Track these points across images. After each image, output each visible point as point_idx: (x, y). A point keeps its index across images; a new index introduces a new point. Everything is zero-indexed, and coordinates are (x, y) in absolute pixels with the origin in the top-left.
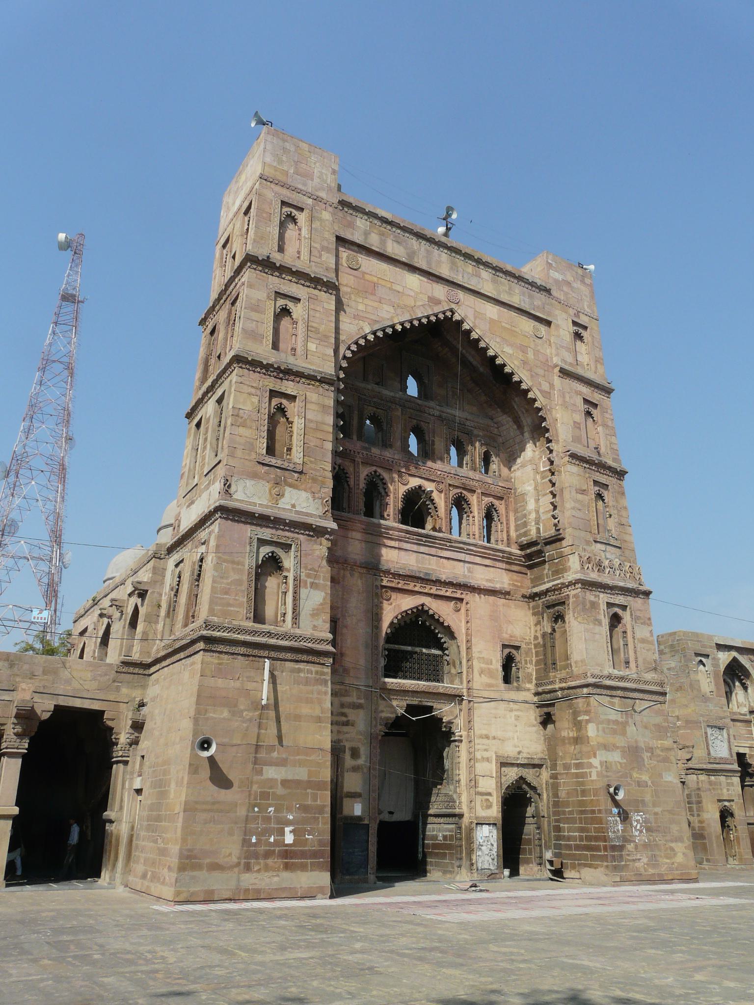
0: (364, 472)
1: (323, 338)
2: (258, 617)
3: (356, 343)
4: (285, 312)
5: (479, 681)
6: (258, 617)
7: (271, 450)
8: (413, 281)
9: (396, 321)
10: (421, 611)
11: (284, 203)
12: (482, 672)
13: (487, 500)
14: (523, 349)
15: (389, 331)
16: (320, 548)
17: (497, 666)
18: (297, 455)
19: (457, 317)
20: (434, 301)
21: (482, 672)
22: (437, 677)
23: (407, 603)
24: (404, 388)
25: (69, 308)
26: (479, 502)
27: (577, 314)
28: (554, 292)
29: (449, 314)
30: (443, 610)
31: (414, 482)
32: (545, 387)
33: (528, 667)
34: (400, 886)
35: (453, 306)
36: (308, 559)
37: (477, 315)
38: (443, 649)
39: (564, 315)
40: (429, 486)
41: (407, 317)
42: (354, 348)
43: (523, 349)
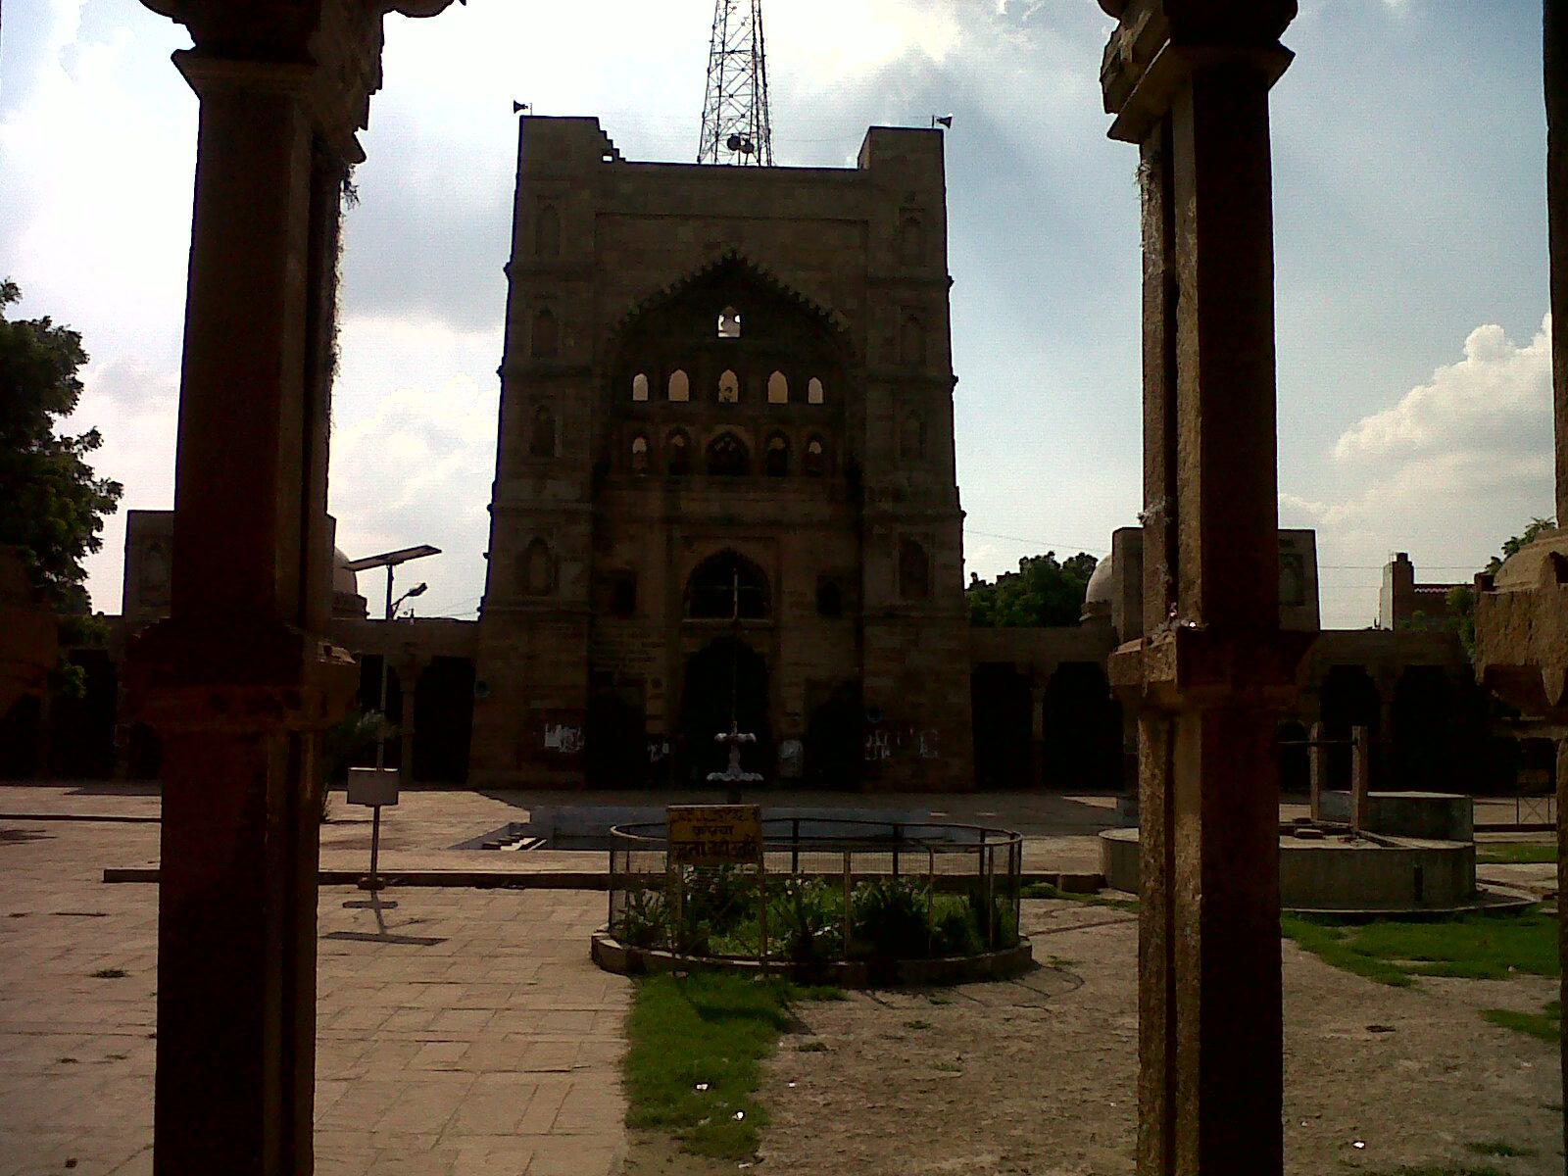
31: (720, 429)
40: (740, 431)
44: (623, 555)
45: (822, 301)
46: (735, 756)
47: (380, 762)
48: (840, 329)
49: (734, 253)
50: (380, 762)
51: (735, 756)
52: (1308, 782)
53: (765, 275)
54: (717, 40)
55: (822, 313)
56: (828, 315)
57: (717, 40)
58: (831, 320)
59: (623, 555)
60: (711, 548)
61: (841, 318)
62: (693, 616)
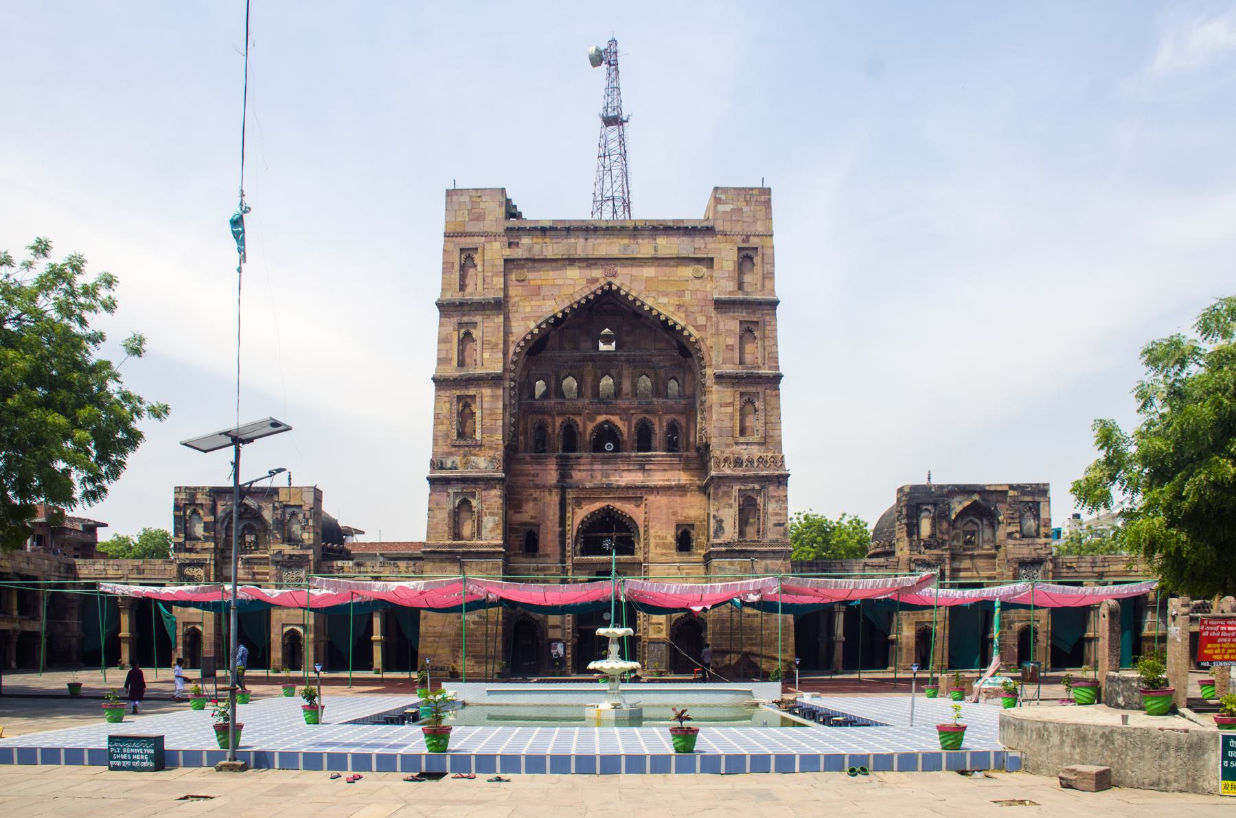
0: (559, 421)
1: (494, 347)
2: (457, 535)
3: (524, 339)
5: (653, 553)
6: (457, 535)
7: (461, 435)
8: (573, 273)
9: (557, 310)
10: (608, 511)
11: (462, 250)
12: (657, 546)
13: (668, 418)
15: (552, 321)
16: (496, 493)
17: (670, 536)
18: (478, 436)
19: (614, 288)
21: (657, 546)
26: (660, 421)
28: (718, 228)
29: (606, 288)
30: (627, 508)
31: (601, 418)
32: (701, 320)
33: (698, 538)
35: (609, 279)
36: (490, 503)
37: (633, 279)
38: (628, 531)
39: (729, 246)
40: (616, 419)
41: (567, 303)
42: (522, 344)
43: (680, 294)
44: (528, 513)
45: (679, 319)
46: (614, 649)
47: (498, 769)
48: (692, 339)
49: (610, 284)
50: (498, 769)
51: (614, 649)
52: (917, 764)
53: (635, 299)
54: (598, 192)
55: (678, 328)
56: (683, 329)
57: (598, 192)
58: (685, 333)
59: (528, 513)
60: (598, 505)
61: (691, 330)
62: (582, 555)
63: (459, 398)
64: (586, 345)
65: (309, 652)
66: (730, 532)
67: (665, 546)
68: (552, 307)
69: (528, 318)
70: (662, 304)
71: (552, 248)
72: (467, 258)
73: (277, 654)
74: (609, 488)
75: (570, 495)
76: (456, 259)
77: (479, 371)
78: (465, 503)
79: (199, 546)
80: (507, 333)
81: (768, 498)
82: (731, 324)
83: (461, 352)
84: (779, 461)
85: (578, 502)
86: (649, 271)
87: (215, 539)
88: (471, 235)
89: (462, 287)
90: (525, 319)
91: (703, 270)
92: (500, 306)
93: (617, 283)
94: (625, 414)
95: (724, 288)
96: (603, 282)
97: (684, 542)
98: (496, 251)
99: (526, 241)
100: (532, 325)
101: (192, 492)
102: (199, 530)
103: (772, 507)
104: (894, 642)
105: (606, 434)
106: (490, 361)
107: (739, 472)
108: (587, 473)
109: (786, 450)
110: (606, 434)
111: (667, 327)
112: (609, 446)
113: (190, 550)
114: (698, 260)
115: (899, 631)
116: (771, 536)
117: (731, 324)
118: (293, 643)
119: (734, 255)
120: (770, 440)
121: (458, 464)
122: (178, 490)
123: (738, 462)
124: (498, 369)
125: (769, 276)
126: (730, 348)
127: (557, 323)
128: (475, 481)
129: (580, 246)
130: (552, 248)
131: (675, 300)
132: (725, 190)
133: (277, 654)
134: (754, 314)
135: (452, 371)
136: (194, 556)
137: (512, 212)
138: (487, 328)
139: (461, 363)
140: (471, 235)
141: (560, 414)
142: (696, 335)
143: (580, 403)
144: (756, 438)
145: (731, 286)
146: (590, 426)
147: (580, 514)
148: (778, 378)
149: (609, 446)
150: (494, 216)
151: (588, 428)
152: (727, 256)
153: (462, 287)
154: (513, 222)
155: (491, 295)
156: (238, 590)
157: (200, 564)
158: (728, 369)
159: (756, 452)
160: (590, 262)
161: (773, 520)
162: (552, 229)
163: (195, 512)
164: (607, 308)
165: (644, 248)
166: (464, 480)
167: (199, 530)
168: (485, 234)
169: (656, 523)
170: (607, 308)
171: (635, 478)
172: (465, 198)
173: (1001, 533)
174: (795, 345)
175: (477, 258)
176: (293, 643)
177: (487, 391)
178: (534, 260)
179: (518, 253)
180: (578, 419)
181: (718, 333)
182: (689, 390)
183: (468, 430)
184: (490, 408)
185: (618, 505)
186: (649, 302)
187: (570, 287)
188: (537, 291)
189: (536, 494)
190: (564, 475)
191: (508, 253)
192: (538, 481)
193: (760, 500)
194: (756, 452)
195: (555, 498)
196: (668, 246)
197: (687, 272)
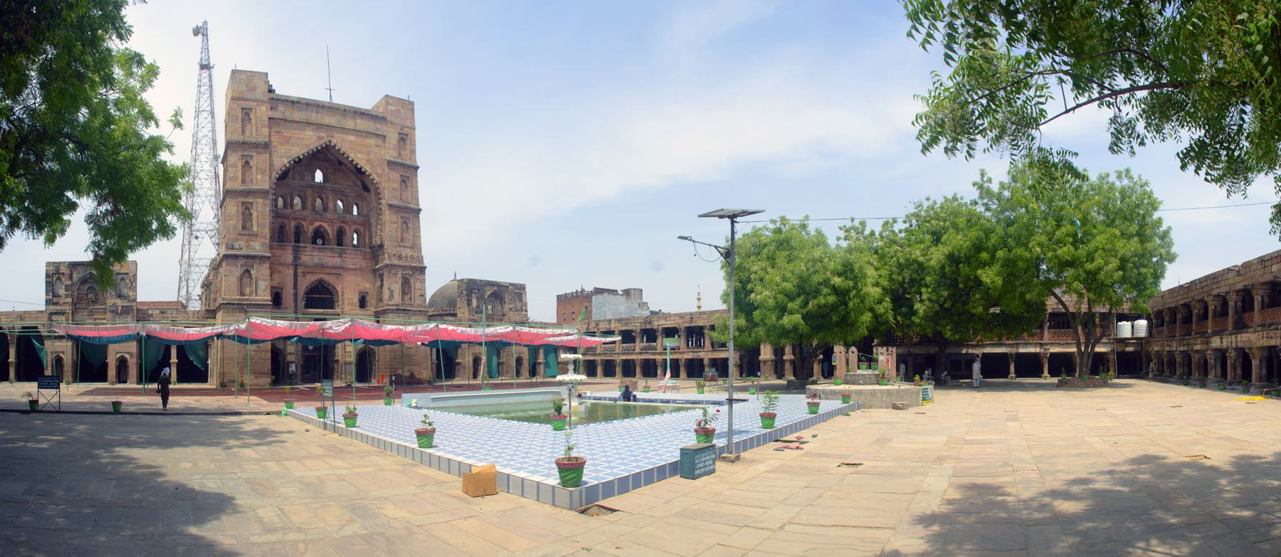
0: (293, 224)
1: (263, 173)
2: (242, 294)
4: (247, 163)
5: (347, 309)
6: (242, 294)
7: (244, 228)
10: (321, 282)
14: (368, 153)
17: (356, 301)
18: (255, 228)
20: (320, 138)
22: (332, 308)
23: (314, 278)
24: (314, 178)
25: (205, 74)
27: (403, 128)
30: (330, 279)
31: (317, 224)
32: (380, 171)
33: (371, 301)
34: (1219, 456)
40: (325, 225)
43: (368, 153)
45: (367, 168)
63: (243, 203)
64: (308, 178)
65: (133, 371)
66: (397, 299)
67: (352, 304)
68: (298, 151)
69: (283, 156)
70: (359, 158)
71: (297, 115)
72: (246, 113)
73: (112, 372)
74: (322, 266)
75: (300, 270)
76: (239, 114)
77: (255, 187)
78: (247, 271)
79: (61, 301)
80: (271, 165)
81: (416, 279)
82: (396, 176)
83: (243, 174)
84: (420, 259)
85: (304, 274)
86: (351, 138)
87: (72, 296)
88: (248, 100)
89: (243, 132)
90: (281, 157)
91: (380, 142)
92: (266, 146)
93: (334, 141)
94: (331, 221)
95: (391, 155)
96: (326, 140)
97: (363, 303)
98: (263, 112)
99: (281, 108)
100: (286, 161)
101: (57, 265)
102: (62, 292)
103: (418, 285)
104: (459, 364)
105: (319, 235)
106: (262, 181)
107: (401, 263)
108: (311, 256)
109: (424, 253)
110: (319, 235)
111: (359, 172)
112: (319, 241)
113: (56, 304)
114: (378, 135)
115: (463, 358)
116: (418, 302)
117: (396, 176)
118: (122, 364)
119: (397, 136)
120: (416, 246)
121: (242, 247)
122: (48, 264)
123: (400, 257)
124: (266, 186)
125: (413, 152)
126: (395, 189)
127: (298, 162)
128: (254, 257)
129: (314, 117)
130: (297, 115)
131: (365, 157)
132: (392, 98)
133: (112, 372)
134: (408, 172)
135: (237, 185)
136: (58, 308)
137: (271, 91)
138: (259, 160)
139: (243, 181)
140: (248, 100)
141: (294, 219)
142: (377, 179)
143: (306, 213)
144: (408, 244)
145: (395, 154)
146: (311, 229)
147: (305, 282)
148: (420, 210)
149: (319, 241)
150: (261, 93)
151: (310, 229)
152: (393, 137)
153: (243, 132)
154: (272, 95)
155: (262, 140)
156: (88, 330)
157: (62, 313)
158: (394, 202)
159: (409, 252)
160: (319, 126)
161: (418, 293)
162: (298, 102)
163: (59, 279)
164: (326, 157)
165: (349, 124)
166: (247, 257)
167: (62, 292)
168: (257, 101)
169: (348, 289)
170: (326, 157)
171: (337, 261)
172: (244, 76)
173: (507, 307)
174: (428, 191)
175: (252, 116)
176: (122, 364)
177: (260, 201)
178: (285, 120)
179: (277, 115)
180: (347, 228)
181: (389, 180)
182: (365, 212)
183: (248, 225)
184: (262, 212)
185: (326, 278)
186: (352, 156)
187: (307, 141)
188: (288, 140)
189: (280, 268)
190: (296, 258)
191: (270, 114)
192: (281, 260)
193: (412, 281)
194: (409, 252)
195: (291, 272)
196: (363, 124)
197: (372, 141)
